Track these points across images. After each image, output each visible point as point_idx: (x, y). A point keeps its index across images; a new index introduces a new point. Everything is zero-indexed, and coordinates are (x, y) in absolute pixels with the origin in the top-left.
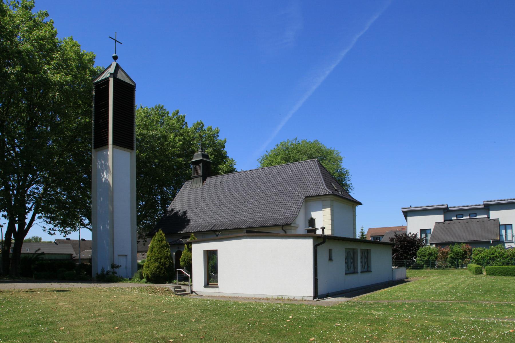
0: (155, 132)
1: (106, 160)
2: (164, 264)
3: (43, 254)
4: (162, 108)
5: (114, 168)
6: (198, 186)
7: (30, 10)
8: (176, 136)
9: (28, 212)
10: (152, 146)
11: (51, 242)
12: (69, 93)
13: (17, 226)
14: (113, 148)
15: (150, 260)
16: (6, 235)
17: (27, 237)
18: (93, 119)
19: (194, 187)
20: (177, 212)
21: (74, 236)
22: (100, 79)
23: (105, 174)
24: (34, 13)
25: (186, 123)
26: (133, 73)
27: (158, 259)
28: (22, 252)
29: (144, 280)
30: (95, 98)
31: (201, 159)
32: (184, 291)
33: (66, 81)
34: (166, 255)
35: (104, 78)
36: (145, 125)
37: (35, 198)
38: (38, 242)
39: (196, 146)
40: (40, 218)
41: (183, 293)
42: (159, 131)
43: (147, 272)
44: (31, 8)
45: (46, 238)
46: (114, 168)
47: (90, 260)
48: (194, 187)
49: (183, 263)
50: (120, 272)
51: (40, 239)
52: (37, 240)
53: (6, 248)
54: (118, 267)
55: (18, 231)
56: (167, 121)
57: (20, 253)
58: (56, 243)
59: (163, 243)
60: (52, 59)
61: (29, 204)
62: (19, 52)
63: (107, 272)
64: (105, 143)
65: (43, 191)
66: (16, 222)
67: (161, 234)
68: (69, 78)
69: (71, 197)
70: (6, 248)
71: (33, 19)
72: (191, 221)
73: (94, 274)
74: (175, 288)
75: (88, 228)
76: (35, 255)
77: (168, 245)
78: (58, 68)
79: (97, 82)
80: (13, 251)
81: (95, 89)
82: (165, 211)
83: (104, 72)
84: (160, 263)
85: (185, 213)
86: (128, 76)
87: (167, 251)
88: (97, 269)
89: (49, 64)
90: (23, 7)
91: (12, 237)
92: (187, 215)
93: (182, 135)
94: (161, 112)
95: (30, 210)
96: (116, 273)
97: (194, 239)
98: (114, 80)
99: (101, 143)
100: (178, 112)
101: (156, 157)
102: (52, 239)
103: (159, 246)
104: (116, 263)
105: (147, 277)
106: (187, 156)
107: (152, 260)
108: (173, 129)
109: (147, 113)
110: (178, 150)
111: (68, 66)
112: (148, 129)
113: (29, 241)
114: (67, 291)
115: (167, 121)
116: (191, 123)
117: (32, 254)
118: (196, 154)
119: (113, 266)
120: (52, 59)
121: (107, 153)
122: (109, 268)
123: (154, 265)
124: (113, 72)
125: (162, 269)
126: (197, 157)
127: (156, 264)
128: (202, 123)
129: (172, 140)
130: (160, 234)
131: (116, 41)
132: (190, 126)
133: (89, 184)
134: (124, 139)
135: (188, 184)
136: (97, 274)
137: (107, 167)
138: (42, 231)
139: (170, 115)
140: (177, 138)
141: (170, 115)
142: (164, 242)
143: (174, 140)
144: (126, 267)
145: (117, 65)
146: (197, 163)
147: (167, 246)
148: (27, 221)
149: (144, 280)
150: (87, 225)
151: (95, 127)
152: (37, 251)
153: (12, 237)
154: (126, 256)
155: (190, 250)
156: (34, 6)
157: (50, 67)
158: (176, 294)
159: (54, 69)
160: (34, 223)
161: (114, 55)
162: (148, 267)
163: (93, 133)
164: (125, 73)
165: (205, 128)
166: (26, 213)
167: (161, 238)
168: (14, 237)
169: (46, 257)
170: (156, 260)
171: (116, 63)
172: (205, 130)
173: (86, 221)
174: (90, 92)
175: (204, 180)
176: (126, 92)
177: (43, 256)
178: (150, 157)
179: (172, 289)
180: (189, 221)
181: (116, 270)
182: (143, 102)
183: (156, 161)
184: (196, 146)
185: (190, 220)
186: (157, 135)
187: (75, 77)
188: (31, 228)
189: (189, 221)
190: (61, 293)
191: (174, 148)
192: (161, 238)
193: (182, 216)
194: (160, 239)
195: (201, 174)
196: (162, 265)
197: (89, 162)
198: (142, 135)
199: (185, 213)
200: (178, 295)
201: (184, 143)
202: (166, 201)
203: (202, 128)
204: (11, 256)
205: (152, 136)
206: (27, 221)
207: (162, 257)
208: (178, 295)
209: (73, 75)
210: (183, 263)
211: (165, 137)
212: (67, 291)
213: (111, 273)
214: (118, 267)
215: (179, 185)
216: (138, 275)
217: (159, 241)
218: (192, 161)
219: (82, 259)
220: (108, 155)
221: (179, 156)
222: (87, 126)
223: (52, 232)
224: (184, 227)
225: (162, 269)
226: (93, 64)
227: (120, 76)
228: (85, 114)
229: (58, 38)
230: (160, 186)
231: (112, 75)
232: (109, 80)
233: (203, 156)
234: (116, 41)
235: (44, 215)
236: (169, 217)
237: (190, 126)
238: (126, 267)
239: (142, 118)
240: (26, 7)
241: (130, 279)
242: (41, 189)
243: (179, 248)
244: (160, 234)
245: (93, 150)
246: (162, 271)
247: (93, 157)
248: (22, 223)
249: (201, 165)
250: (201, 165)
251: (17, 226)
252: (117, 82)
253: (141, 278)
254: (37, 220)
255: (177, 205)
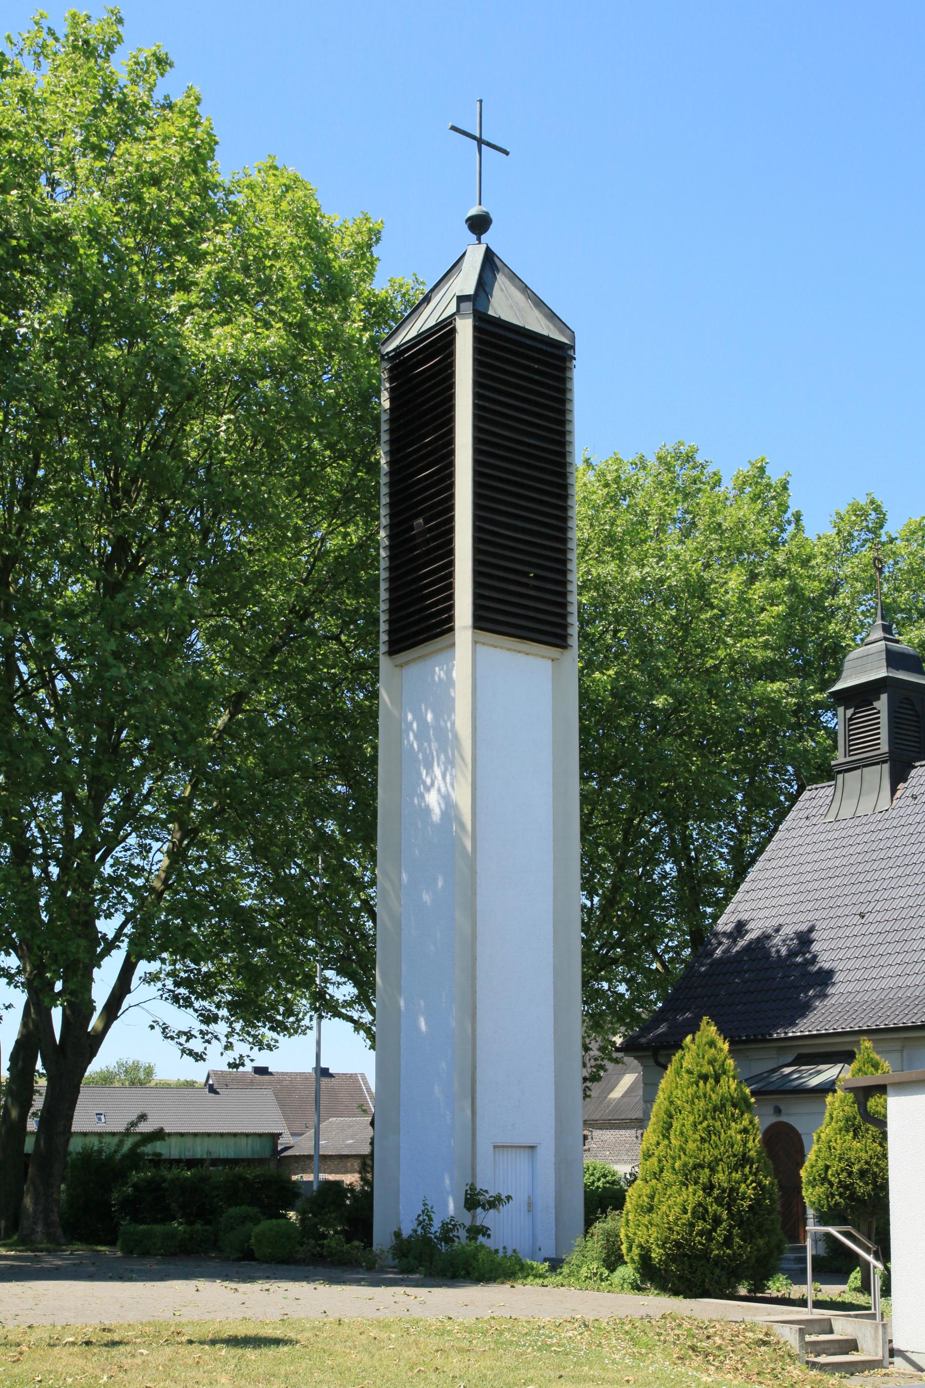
0: (652, 569)
1: (445, 707)
2: (729, 1197)
3: (159, 1135)
4: (689, 458)
5: (480, 746)
6: (866, 807)
7: (107, 59)
8: (753, 578)
9: (107, 952)
10: (640, 636)
11: (190, 1085)
12: (277, 402)
13: (57, 1015)
14: (475, 642)
15: (657, 1176)
16: (14, 1058)
17: (95, 1067)
18: (384, 521)
19: (846, 813)
20: (766, 937)
21: (290, 1055)
22: (413, 333)
23: (437, 771)
24: (120, 66)
25: (798, 517)
26: (561, 282)
27: (698, 1166)
28: (75, 1128)
29: (627, 1271)
30: (391, 421)
31: (882, 673)
32: (851, 1346)
33: (263, 354)
34: (738, 1148)
35: (431, 323)
36: (610, 539)
37: (133, 889)
38: (142, 1084)
39: (846, 619)
40: (152, 978)
41: (842, 1356)
42: (674, 558)
43: (641, 1237)
44: (110, 48)
45: (171, 1066)
46: (480, 746)
47: (366, 1163)
48: (846, 813)
49: (820, 1190)
50: (505, 1230)
51: (149, 1071)
52: (137, 1078)
53: (14, 1114)
54: (494, 1203)
55: (61, 1049)
56: (714, 513)
57: (68, 1133)
58: (212, 1090)
59: (722, 1089)
60: (197, 258)
61: (109, 916)
62: (59, 236)
63: (444, 1225)
64: (439, 625)
65: (166, 862)
66: (54, 998)
67: (712, 1044)
68: (274, 338)
69: (280, 886)
70: (14, 1114)
71: (116, 95)
72: (837, 978)
73: (382, 1237)
74: (805, 1327)
75: (350, 1019)
76: (128, 1143)
77: (745, 1100)
78: (225, 296)
79: (399, 352)
80: (41, 1125)
81: (391, 380)
82: (700, 938)
83: (427, 299)
84: (709, 1188)
85: (805, 939)
86: (539, 303)
87: (745, 1131)
88: (394, 1217)
89: (184, 285)
90: (75, 48)
91: (39, 1066)
92: (815, 947)
93: (778, 573)
94: (683, 476)
95: (111, 946)
96: (483, 1231)
97: (876, 1066)
98: (475, 328)
99: (419, 623)
100: (762, 470)
101: (659, 684)
102: (197, 1073)
103: (701, 1104)
104: (489, 1185)
105: (645, 1261)
106: (803, 671)
107: (667, 1176)
108: (738, 550)
109: (617, 480)
110: (766, 646)
111: (266, 286)
112: (620, 557)
113: (106, 1079)
114: (277, 1342)
115: (714, 513)
116: (818, 517)
117: (113, 1134)
118: (851, 656)
119: (473, 1201)
120: (197, 258)
121: (449, 673)
122: (452, 1207)
123: (680, 1201)
124: (470, 290)
125: (717, 1221)
126: (864, 666)
127: (692, 1196)
128: (878, 509)
129: (731, 597)
130: (706, 1044)
131: (480, 142)
132: (818, 527)
133: (363, 826)
134: (525, 604)
135: (816, 798)
136: (398, 1235)
137: (445, 739)
138: (157, 1051)
139: (728, 485)
140: (760, 588)
141: (728, 485)
142: (729, 1086)
143: (743, 599)
144: (530, 1206)
145: (490, 259)
146: (860, 697)
147: (741, 1104)
148: (101, 992)
149: (627, 1271)
150: (349, 1004)
151: (391, 558)
152: (133, 1124)
153: (39, 1066)
154: (532, 1148)
155: (869, 1122)
156: (120, 40)
157: (194, 297)
158: (813, 1365)
159: (206, 306)
160: (128, 1000)
161: (474, 211)
162: (651, 1209)
163: (383, 586)
164: (525, 289)
165: (893, 527)
166: (96, 961)
167: (711, 1062)
168: (44, 1065)
169: (170, 1150)
170: (688, 1176)
171: (483, 248)
172: (892, 540)
173: (344, 991)
174: (368, 395)
175: (899, 776)
176: (530, 375)
177: (158, 1147)
178: (630, 687)
179: (789, 1336)
180: (826, 978)
181: (484, 1217)
182: (605, 433)
183: (660, 702)
184: (846, 619)
185: (830, 973)
186: (661, 581)
187: (300, 332)
188: (116, 1024)
189: (826, 978)
190: (251, 1354)
191: (743, 635)
192: (711, 1062)
193: (792, 954)
194: (707, 1069)
195: (884, 747)
196: (718, 1201)
197: (367, 720)
198: (598, 585)
199: (805, 939)
200: (823, 1367)
201: (792, 611)
202: (702, 890)
203: (875, 531)
204: (29, 1145)
205: (642, 589)
206: (101, 992)
207: (717, 1161)
208: (823, 1367)
209: (288, 325)
210: (820, 1190)
211: (699, 590)
212: (277, 1342)
213: (463, 1234)
214: (494, 1203)
215: (771, 808)
216: (596, 1245)
217: (705, 1078)
218: (838, 687)
219: (325, 1158)
220: (450, 683)
221: (769, 671)
222: (349, 567)
223: (196, 1045)
224: (804, 1009)
225: (717, 1221)
226: (371, 274)
227: (506, 305)
228: (349, 504)
229: (224, 169)
230: (675, 818)
231: (467, 307)
232: (453, 331)
233: (894, 659)
234: (480, 142)
235: (168, 968)
236: (729, 961)
237: (818, 527)
238: (530, 1206)
239: (596, 508)
240: (87, 49)
241: (555, 1265)
242: (159, 858)
243: (778, 1111)
244: (706, 1044)
245: (385, 663)
246: (720, 1234)
247: (384, 695)
248: (79, 1008)
249: (882, 703)
250: (882, 703)
251: (57, 1015)
252: (491, 333)
253: (613, 1260)
254: (139, 991)
255: (764, 904)
